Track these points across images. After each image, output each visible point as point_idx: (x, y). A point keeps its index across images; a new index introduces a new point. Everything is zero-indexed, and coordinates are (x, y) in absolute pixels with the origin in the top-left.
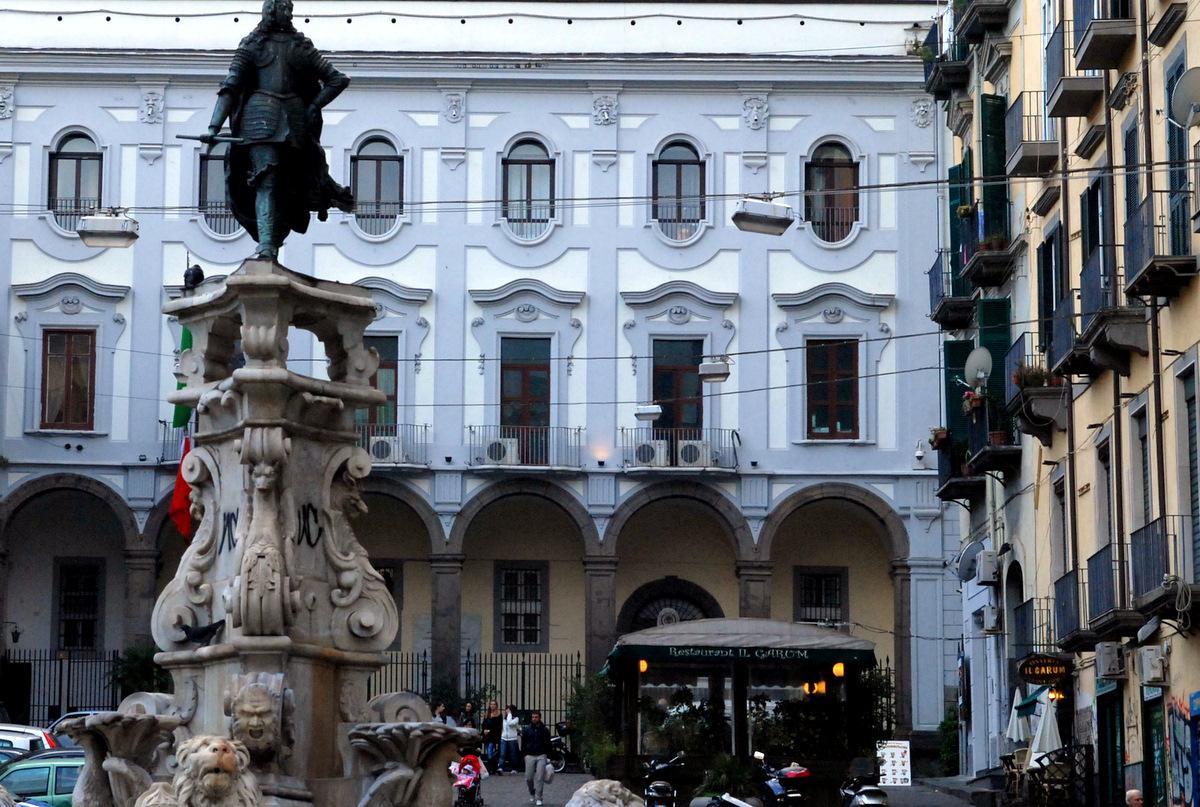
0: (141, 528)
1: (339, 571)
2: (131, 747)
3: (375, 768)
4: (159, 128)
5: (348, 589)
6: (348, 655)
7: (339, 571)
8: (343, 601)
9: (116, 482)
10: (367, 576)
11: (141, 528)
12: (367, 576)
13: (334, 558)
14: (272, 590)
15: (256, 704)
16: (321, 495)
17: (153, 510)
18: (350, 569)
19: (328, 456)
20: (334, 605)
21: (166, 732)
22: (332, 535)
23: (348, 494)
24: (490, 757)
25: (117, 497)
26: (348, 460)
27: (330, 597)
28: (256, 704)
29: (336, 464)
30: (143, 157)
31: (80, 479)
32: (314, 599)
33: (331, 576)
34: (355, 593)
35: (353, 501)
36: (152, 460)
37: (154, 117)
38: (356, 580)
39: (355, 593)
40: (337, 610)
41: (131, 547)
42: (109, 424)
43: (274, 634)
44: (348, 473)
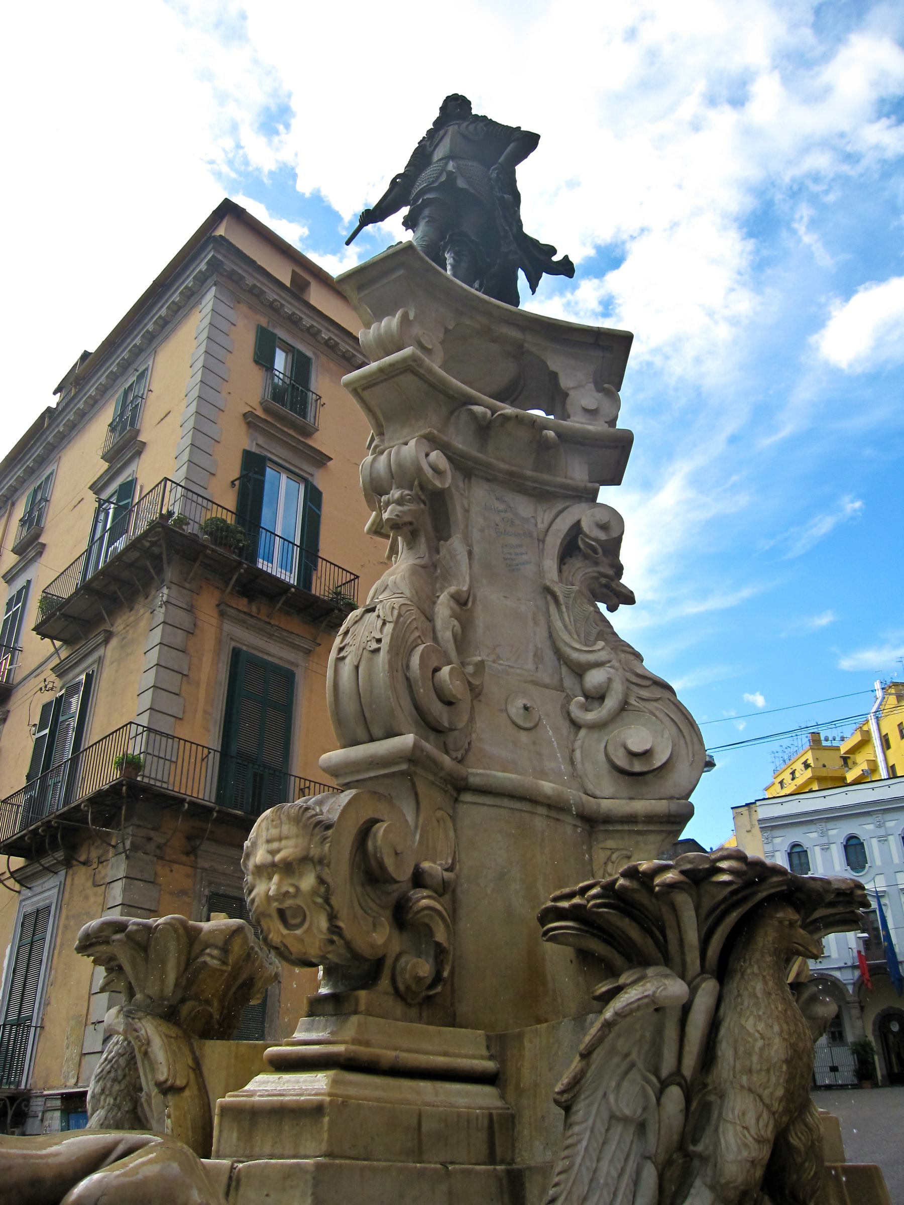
0: (851, 992)
1: (579, 671)
2: (163, 981)
3: (603, 988)
4: (825, 838)
5: (597, 697)
6: (607, 805)
7: (579, 671)
8: (590, 716)
9: (837, 974)
10: (634, 679)
11: (851, 992)
12: (634, 679)
13: (569, 651)
14: (378, 650)
15: (275, 845)
16: (539, 565)
17: (854, 984)
18: (598, 665)
19: (548, 517)
20: (576, 725)
21: (215, 952)
22: (563, 620)
23: (595, 569)
24: (251, 169)
25: (839, 980)
26: (579, 522)
27: (569, 714)
28: (275, 845)
29: (563, 525)
30: (823, 849)
31: (822, 974)
32: (526, 708)
33: (569, 681)
34: (611, 703)
35: (603, 581)
36: (849, 964)
37: (823, 834)
38: (610, 680)
39: (611, 703)
40: (582, 733)
41: (848, 999)
42: (830, 952)
43: (391, 734)
44: (586, 536)
